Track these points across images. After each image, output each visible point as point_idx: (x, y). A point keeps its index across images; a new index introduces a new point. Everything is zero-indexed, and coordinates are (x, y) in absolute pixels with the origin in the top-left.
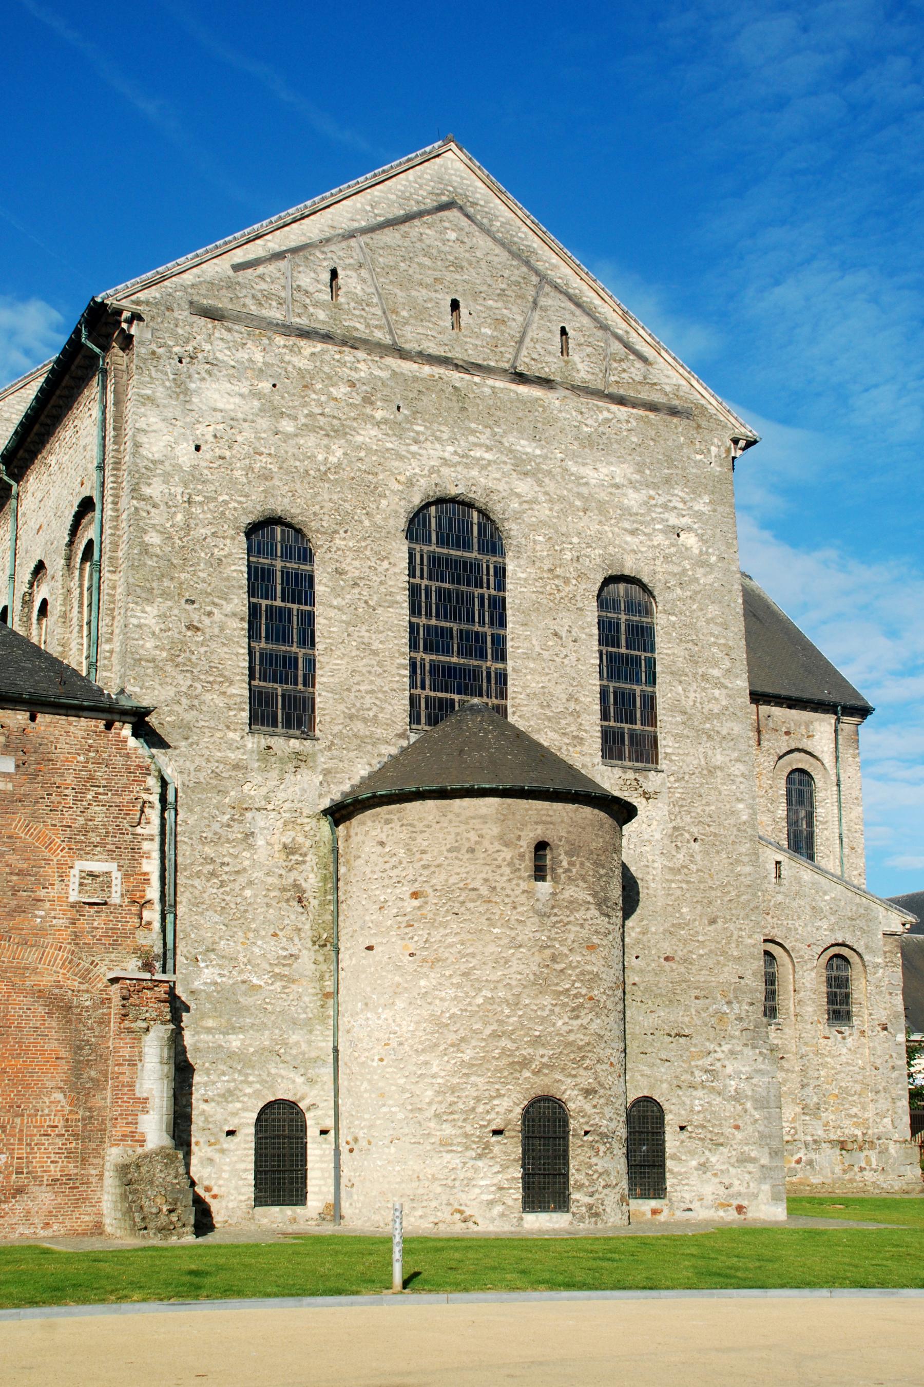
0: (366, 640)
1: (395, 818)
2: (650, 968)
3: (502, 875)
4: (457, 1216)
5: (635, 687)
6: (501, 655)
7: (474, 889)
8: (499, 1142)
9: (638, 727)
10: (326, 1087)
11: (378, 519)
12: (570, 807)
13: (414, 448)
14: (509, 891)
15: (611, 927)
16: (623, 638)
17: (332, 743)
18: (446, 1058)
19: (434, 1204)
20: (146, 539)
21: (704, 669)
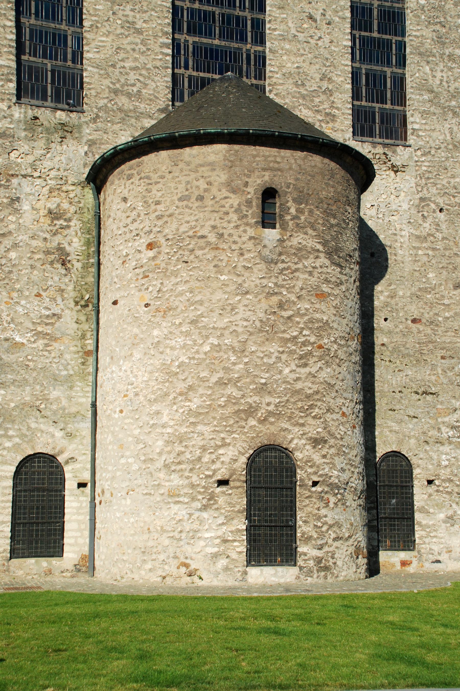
0: (130, 19)
1: (135, 172)
2: (398, 330)
3: (229, 222)
4: (183, 570)
5: (385, 69)
6: (260, 39)
7: (203, 237)
8: (223, 493)
9: (388, 106)
10: (85, 442)
12: (299, 154)
14: (236, 238)
15: (344, 278)
16: (375, 23)
17: (98, 116)
18: (175, 407)
19: (162, 557)
21: (450, 50)
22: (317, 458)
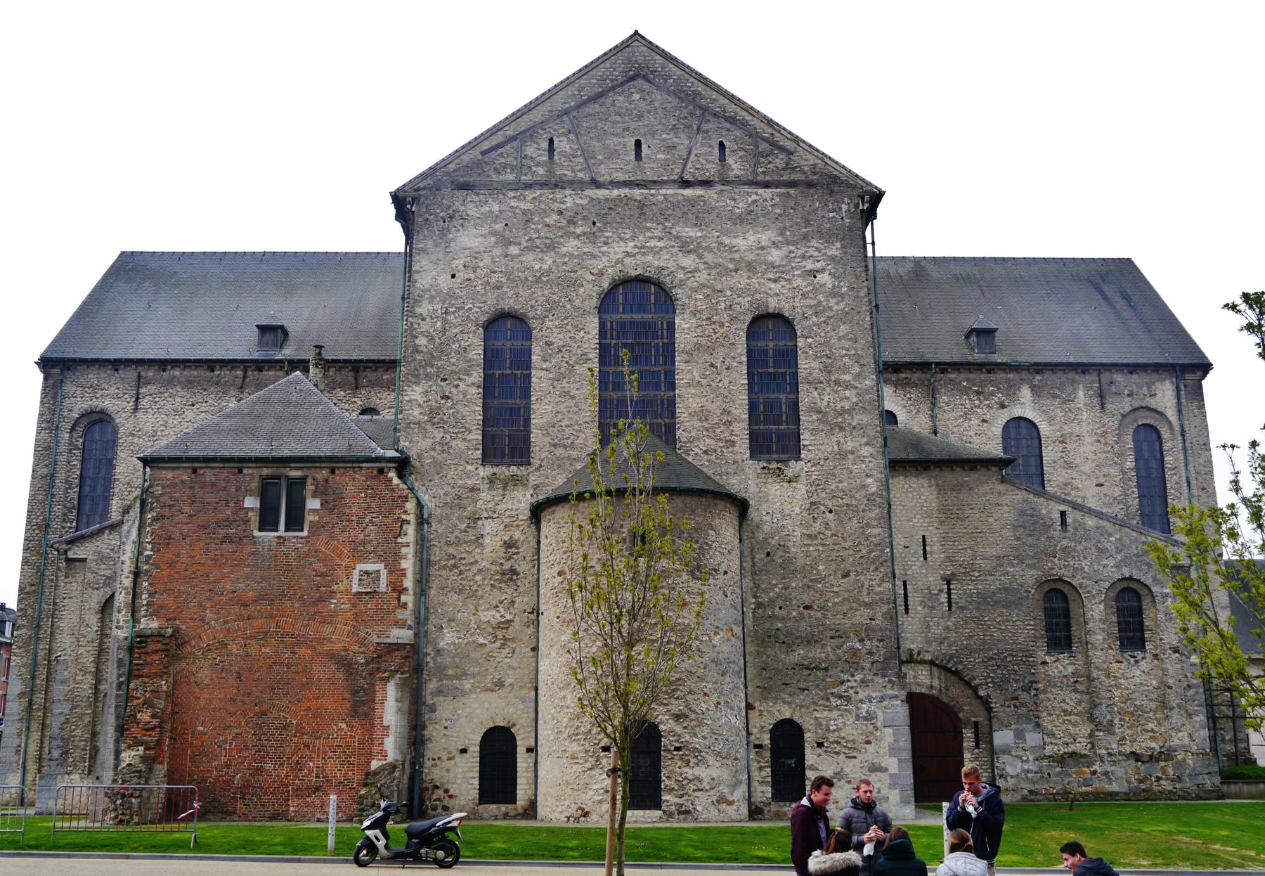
6: (672, 386)
11: (577, 303)
13: (605, 248)
20: (417, 342)
22: (678, 729)
